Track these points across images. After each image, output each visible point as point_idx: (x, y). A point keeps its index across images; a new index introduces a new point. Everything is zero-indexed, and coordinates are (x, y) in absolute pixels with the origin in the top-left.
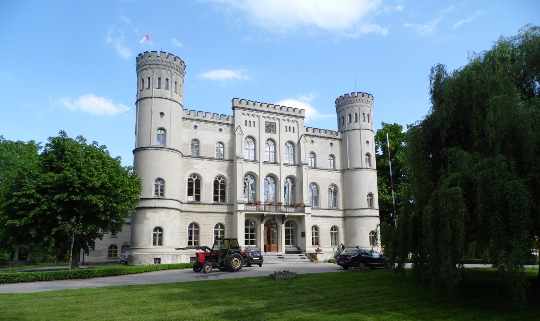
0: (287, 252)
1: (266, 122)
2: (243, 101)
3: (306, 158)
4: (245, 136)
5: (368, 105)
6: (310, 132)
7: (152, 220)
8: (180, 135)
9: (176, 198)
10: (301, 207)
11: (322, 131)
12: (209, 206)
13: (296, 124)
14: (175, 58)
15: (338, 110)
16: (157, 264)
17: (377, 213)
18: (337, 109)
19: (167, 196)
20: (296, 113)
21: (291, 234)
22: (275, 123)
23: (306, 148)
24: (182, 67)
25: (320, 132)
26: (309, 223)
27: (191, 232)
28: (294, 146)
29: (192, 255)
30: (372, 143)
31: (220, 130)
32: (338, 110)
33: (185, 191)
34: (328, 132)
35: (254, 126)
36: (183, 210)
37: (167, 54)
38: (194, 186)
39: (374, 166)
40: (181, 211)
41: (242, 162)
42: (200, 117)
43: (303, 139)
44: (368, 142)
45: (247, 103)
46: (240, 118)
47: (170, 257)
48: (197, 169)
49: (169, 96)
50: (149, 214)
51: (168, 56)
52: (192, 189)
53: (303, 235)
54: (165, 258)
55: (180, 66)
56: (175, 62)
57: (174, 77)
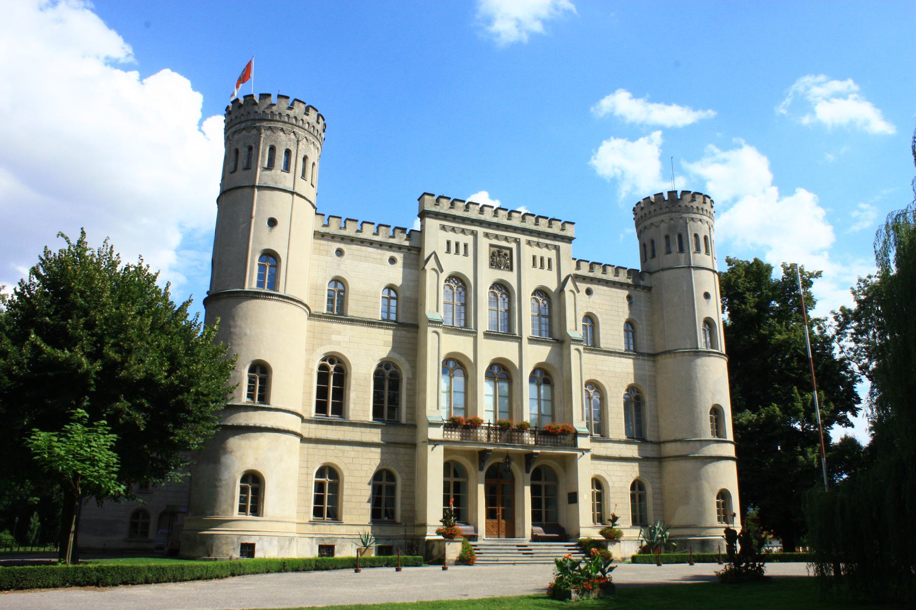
0: (535, 538)
1: (491, 246)
2: (442, 200)
3: (574, 328)
4: (444, 276)
5: (704, 218)
6: (584, 271)
7: (245, 454)
8: (306, 268)
9: (291, 408)
10: (568, 436)
11: (609, 269)
12: (363, 429)
13: (554, 252)
14: (307, 109)
15: (640, 227)
16: (246, 559)
17: (729, 450)
18: (637, 226)
19: (274, 402)
20: (556, 229)
21: (543, 497)
22: (511, 250)
23: (576, 306)
24: (320, 127)
25: (604, 271)
26: (586, 470)
27: (319, 487)
28: (550, 301)
29: (322, 539)
30: (716, 298)
31: (340, 252)
32: (640, 227)
33: (311, 393)
34: (621, 271)
35: (466, 254)
36: (306, 435)
37: (290, 101)
38: (332, 378)
39: (722, 347)
40: (304, 440)
41: (440, 330)
42: (351, 231)
43: (570, 285)
44: (707, 296)
45: (452, 204)
46: (436, 237)
47: (275, 542)
48: (338, 343)
49: (289, 186)
50: (234, 442)
51: (292, 104)
52: (327, 390)
53: (573, 498)
54: (266, 544)
55: (315, 124)
56: (305, 117)
57: (302, 145)
